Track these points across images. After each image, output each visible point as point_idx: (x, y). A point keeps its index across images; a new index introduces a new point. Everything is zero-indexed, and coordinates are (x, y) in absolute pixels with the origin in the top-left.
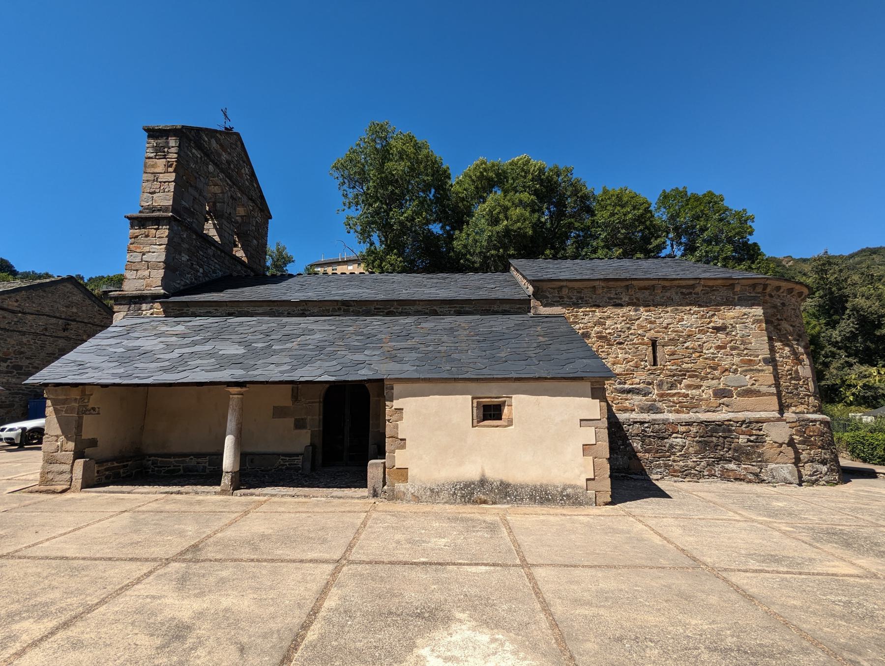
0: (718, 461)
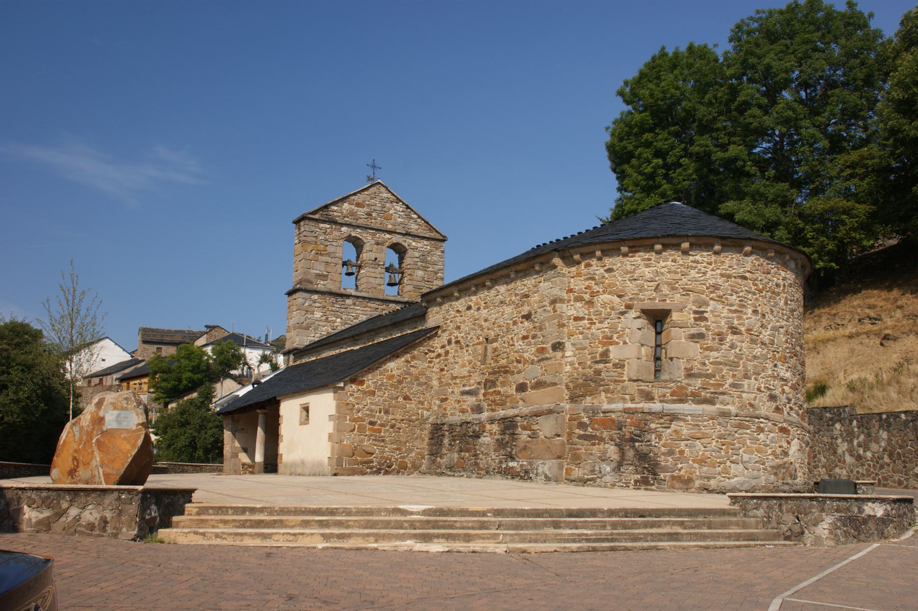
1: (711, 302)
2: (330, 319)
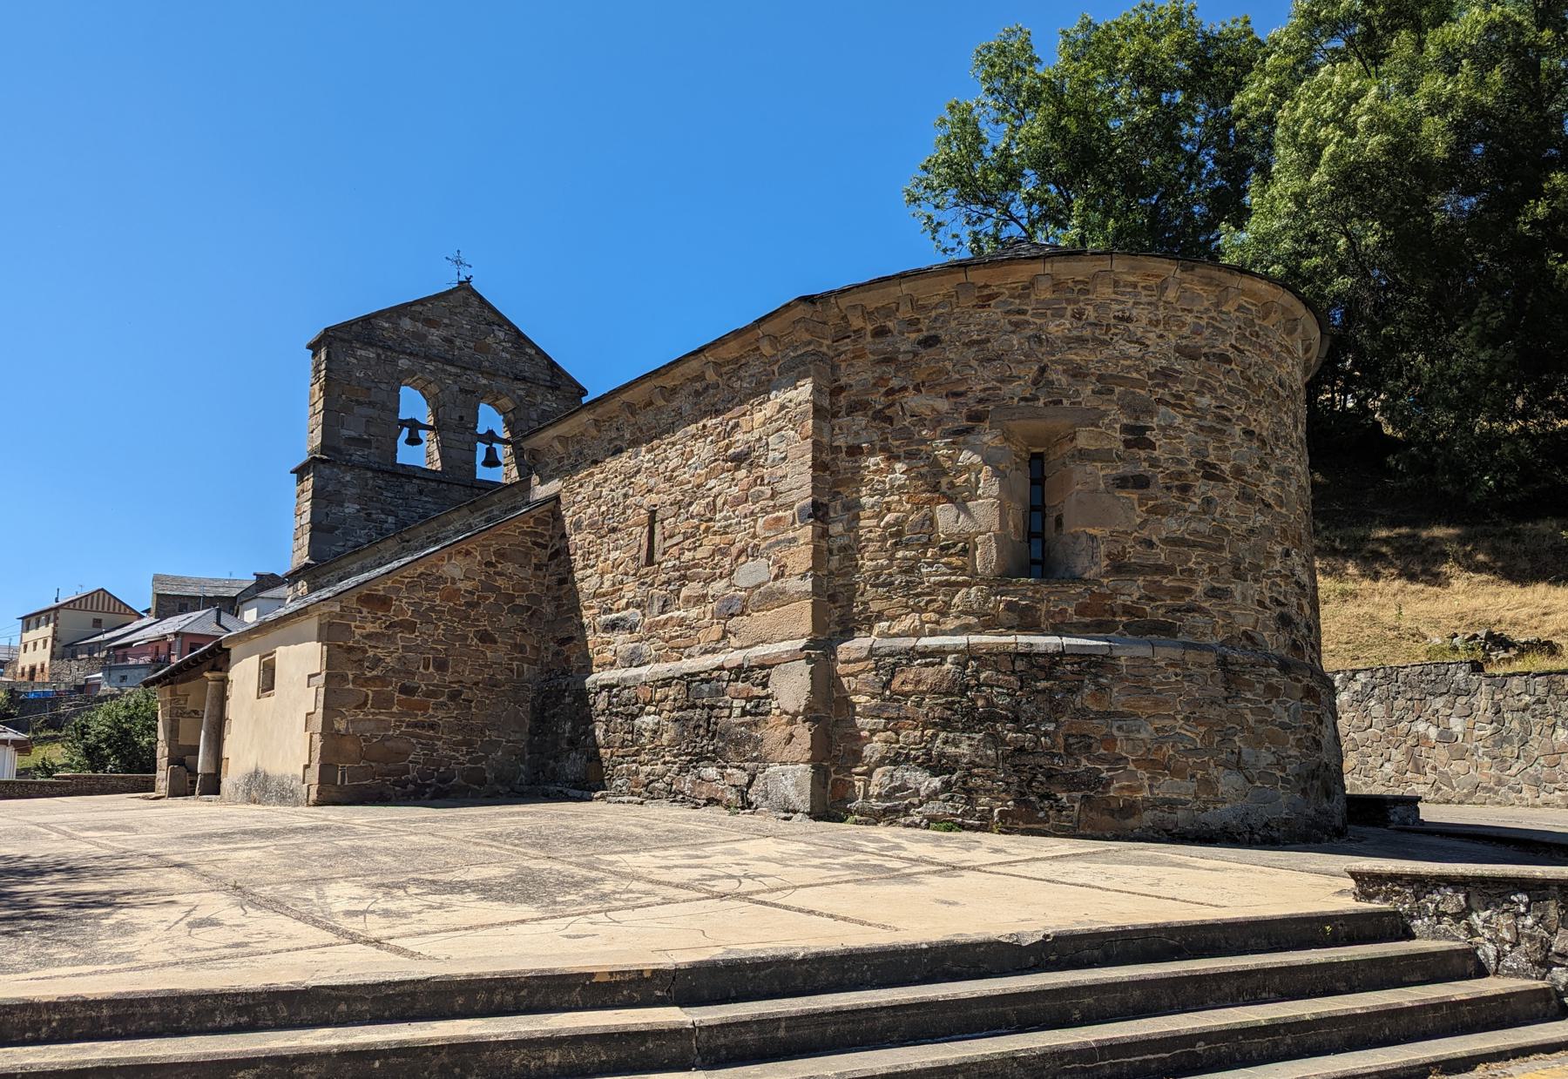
0: (697, 762)
1: (1162, 409)
2: (374, 516)
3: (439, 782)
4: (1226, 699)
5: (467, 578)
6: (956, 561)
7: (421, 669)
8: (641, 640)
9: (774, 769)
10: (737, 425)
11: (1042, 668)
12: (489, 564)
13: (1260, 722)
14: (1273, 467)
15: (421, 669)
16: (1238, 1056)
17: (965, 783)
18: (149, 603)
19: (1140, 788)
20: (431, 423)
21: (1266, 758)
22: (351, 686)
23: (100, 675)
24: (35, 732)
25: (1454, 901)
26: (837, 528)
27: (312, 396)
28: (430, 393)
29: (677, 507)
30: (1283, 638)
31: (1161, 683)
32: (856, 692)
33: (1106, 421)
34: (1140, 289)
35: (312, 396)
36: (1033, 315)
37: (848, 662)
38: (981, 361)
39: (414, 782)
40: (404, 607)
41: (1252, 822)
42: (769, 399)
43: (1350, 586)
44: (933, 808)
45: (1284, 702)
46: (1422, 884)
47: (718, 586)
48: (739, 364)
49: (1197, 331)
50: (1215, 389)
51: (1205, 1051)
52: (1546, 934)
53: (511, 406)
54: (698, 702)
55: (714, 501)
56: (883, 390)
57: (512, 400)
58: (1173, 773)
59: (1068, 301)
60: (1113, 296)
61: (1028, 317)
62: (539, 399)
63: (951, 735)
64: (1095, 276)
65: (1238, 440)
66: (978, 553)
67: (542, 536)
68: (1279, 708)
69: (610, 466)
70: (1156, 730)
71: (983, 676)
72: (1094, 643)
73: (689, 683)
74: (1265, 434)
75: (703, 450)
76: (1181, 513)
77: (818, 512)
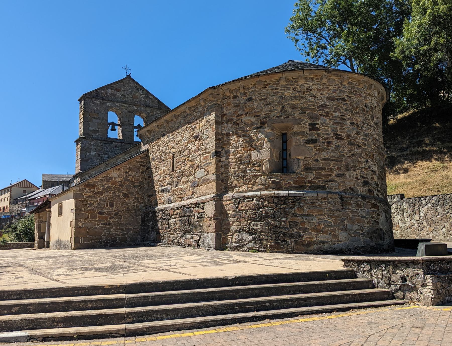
1: (322, 117)
3: (112, 241)
4: (342, 209)
5: (119, 177)
6: (257, 168)
7: (105, 206)
8: (171, 195)
9: (206, 234)
10: (195, 127)
11: (282, 201)
12: (126, 172)
13: (354, 216)
14: (362, 134)
15: (105, 206)
16: (279, 307)
17: (259, 237)
18: (41, 184)
19: (313, 238)
20: (119, 123)
21: (356, 227)
22: (83, 212)
23: (25, 209)
24: (4, 229)
25: (367, 267)
26: (223, 159)
27: (80, 116)
28: (118, 113)
29: (180, 153)
30: (365, 188)
31: (320, 205)
32: (229, 210)
33: (303, 122)
34: (314, 80)
35: (80, 116)
36: (280, 90)
37: (226, 201)
38: (265, 105)
39: (104, 242)
40: (99, 187)
41: (350, 248)
42: (204, 119)
43: (445, 165)
44: (250, 245)
45: (363, 209)
46: (360, 262)
47: (191, 177)
48: (196, 107)
49: (334, 91)
50: (340, 110)
51: (269, 305)
52: (390, 276)
53: (146, 116)
54: (186, 214)
55: (190, 151)
56: (236, 115)
57: (146, 114)
58: (324, 233)
59: (291, 85)
60: (306, 82)
61: (279, 91)
62: (155, 113)
63: (255, 223)
64: (299, 76)
65: (348, 126)
66: (264, 166)
67: (143, 162)
68: (361, 211)
69: (162, 140)
70: (318, 219)
71: (264, 204)
72: (299, 193)
73: (183, 208)
74: (359, 123)
75: (187, 135)
76: (328, 150)
77: (217, 154)
